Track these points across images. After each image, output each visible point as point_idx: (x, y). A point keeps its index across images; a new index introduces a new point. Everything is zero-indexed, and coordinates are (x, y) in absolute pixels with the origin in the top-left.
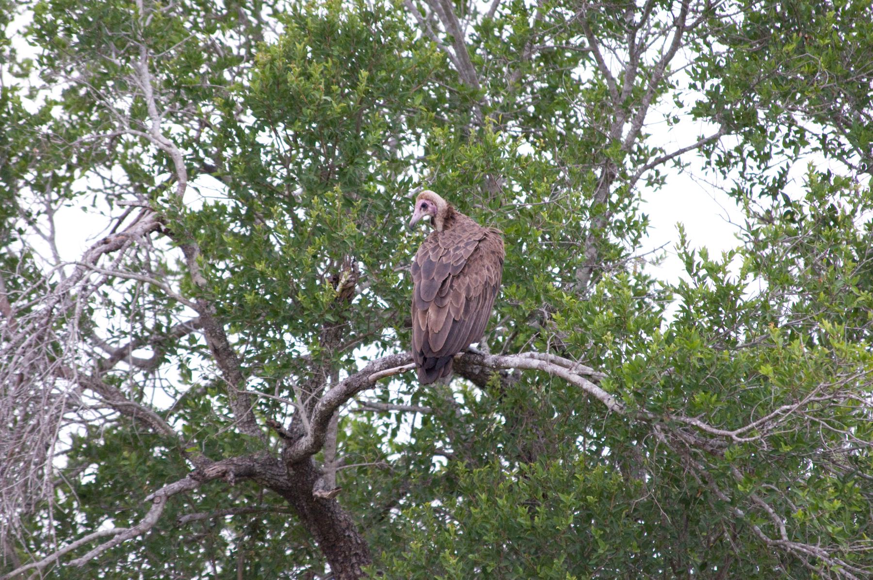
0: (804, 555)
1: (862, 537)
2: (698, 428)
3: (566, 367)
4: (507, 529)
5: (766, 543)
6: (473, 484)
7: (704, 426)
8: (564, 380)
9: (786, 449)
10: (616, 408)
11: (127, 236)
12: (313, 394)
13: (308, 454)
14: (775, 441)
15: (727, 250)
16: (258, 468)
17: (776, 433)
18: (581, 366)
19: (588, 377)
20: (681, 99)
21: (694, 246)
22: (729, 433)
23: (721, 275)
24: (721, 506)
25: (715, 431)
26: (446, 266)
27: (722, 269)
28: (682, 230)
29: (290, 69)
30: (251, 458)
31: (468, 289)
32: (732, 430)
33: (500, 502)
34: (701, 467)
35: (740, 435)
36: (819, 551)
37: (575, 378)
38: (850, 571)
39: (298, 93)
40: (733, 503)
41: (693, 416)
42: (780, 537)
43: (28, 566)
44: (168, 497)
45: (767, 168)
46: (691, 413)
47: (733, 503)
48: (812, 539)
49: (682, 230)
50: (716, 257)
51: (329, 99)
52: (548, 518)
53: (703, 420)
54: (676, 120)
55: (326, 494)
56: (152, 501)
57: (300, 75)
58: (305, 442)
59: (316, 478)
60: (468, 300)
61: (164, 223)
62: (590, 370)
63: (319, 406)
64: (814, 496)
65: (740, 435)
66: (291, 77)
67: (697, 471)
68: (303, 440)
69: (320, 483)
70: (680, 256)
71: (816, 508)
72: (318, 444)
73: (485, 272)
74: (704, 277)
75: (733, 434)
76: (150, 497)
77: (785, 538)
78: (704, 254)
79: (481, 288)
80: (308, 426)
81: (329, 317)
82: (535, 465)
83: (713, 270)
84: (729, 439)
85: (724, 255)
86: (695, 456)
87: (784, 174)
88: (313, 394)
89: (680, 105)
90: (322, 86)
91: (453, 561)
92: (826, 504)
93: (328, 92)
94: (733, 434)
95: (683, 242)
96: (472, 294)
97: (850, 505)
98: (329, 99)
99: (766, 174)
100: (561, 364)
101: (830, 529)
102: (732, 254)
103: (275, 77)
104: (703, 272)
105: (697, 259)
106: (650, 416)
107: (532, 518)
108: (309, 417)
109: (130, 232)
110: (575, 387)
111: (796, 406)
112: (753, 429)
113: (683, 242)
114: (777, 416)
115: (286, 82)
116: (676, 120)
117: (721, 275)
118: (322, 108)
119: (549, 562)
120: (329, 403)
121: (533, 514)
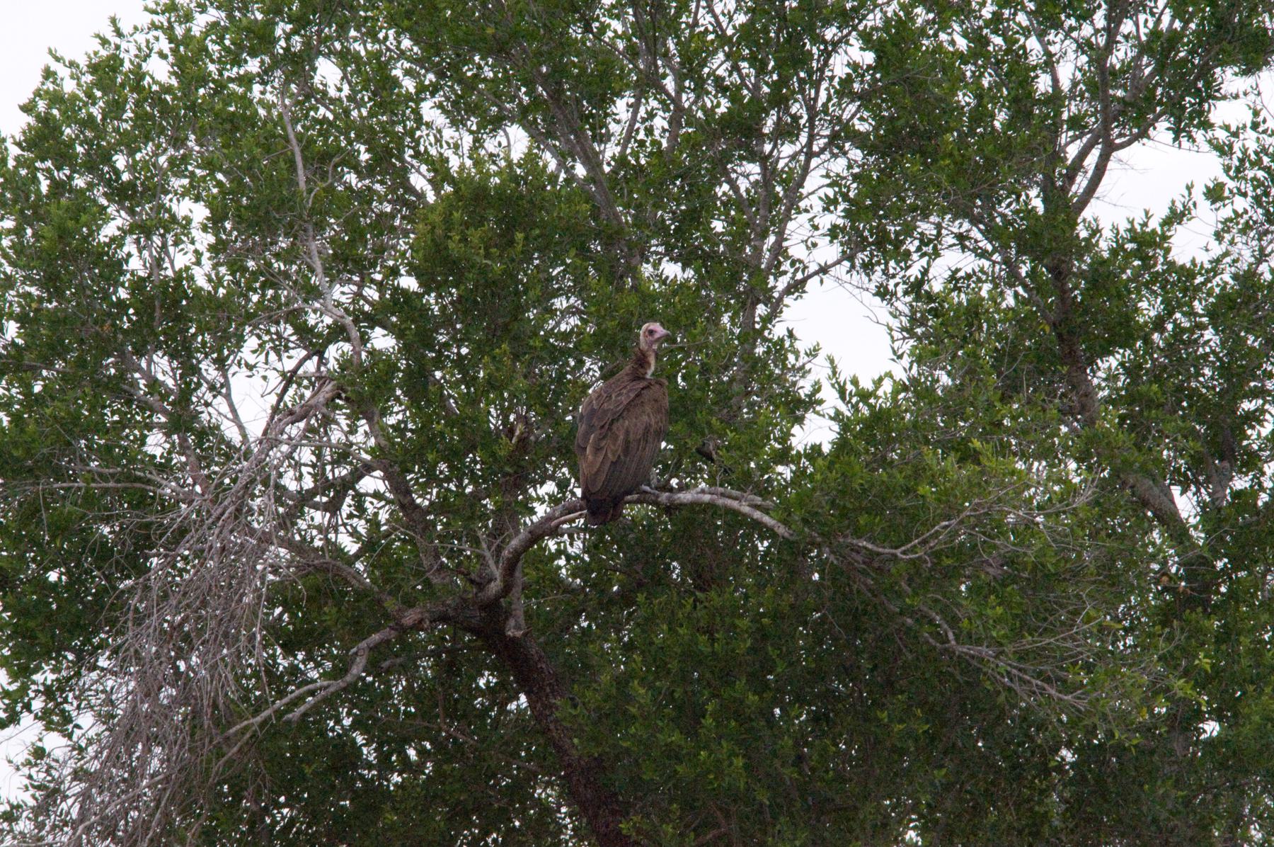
0: (973, 657)
1: (1023, 637)
2: (865, 548)
3: (736, 499)
4: (691, 656)
5: (935, 648)
6: (653, 613)
7: (870, 546)
8: (736, 513)
9: (947, 562)
10: (786, 535)
11: (311, 407)
12: (498, 541)
13: (497, 598)
14: (937, 555)
15: (876, 378)
16: (451, 613)
17: (937, 548)
18: (752, 497)
19: (757, 507)
20: (816, 221)
21: (845, 376)
22: (893, 551)
23: (872, 401)
24: (891, 617)
25: (880, 550)
26: (605, 412)
27: (872, 394)
28: (832, 361)
29: (450, 238)
30: (443, 604)
31: (627, 432)
32: (896, 548)
33: (681, 631)
34: (870, 582)
35: (904, 553)
36: (987, 651)
37: (746, 509)
38: (1015, 668)
39: (460, 260)
40: (901, 613)
41: (859, 538)
42: (948, 641)
43: (246, 723)
44: (371, 649)
45: (908, 268)
46: (858, 533)
47: (901, 613)
48: (979, 642)
49: (832, 361)
50: (866, 384)
51: (489, 262)
52: (727, 644)
53: (869, 540)
54: (815, 245)
55: (519, 634)
56: (356, 654)
57: (460, 241)
58: (495, 587)
59: (507, 618)
60: (627, 442)
61: (345, 392)
62: (758, 500)
63: (506, 553)
64: (979, 604)
65: (904, 553)
66: (451, 245)
67: (866, 585)
68: (493, 584)
69: (512, 622)
70: (833, 385)
71: (981, 615)
72: (507, 589)
73: (645, 418)
74: (857, 403)
75: (898, 552)
76: (354, 650)
77: (953, 643)
78: (855, 382)
79: (641, 432)
80: (497, 572)
81: (508, 469)
82: (713, 594)
83: (865, 396)
84: (895, 556)
85: (874, 382)
86: (864, 572)
87: (925, 272)
88: (498, 541)
89: (816, 228)
90: (482, 251)
91: (642, 691)
92: (989, 612)
93: (487, 255)
94: (898, 552)
95: (834, 373)
96: (631, 437)
97: (1011, 608)
98: (489, 262)
99: (908, 273)
100: (730, 497)
101: (994, 634)
102: (881, 380)
103: (437, 245)
104: (854, 400)
105: (849, 387)
106: (819, 539)
107: (712, 645)
108: (497, 563)
109: (312, 402)
110: (745, 515)
111: (954, 522)
112: (915, 546)
113: (834, 373)
114: (937, 534)
115: (446, 248)
116: (815, 245)
117: (872, 401)
118: (483, 270)
119: (731, 684)
120: (515, 550)
121: (713, 640)
